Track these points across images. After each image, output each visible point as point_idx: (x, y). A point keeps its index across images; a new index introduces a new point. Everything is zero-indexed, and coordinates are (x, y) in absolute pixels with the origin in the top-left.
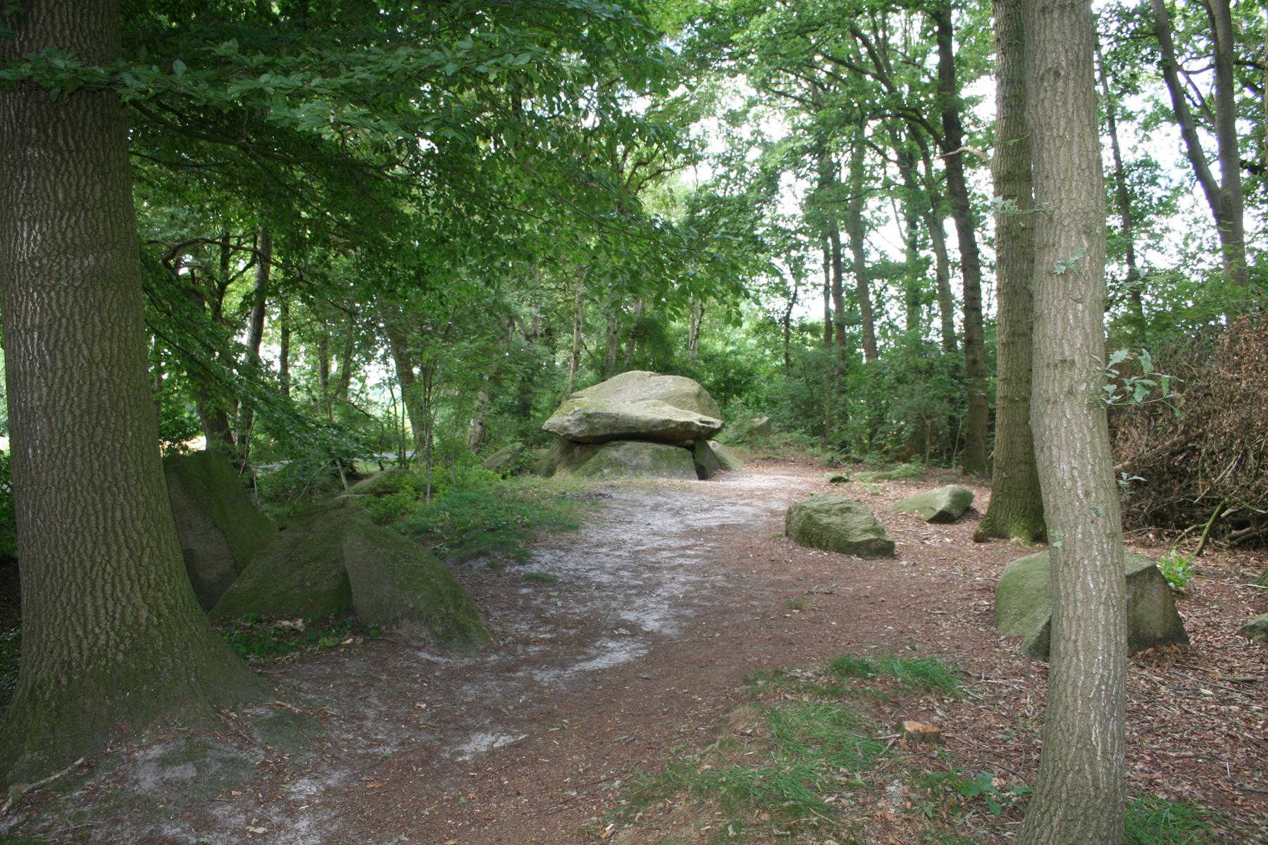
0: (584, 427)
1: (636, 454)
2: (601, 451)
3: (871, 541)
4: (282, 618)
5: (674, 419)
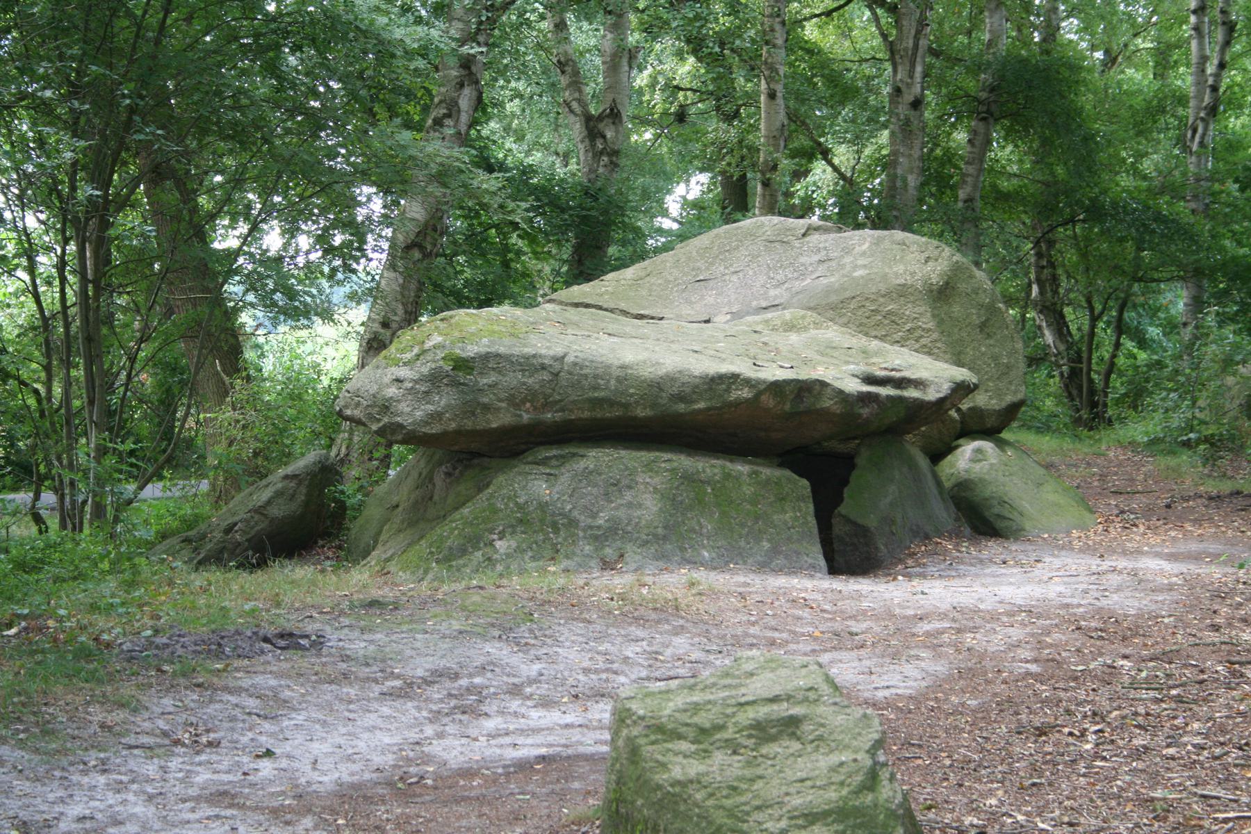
0: (444, 400)
1: (615, 487)
2: (501, 479)
5: (742, 368)
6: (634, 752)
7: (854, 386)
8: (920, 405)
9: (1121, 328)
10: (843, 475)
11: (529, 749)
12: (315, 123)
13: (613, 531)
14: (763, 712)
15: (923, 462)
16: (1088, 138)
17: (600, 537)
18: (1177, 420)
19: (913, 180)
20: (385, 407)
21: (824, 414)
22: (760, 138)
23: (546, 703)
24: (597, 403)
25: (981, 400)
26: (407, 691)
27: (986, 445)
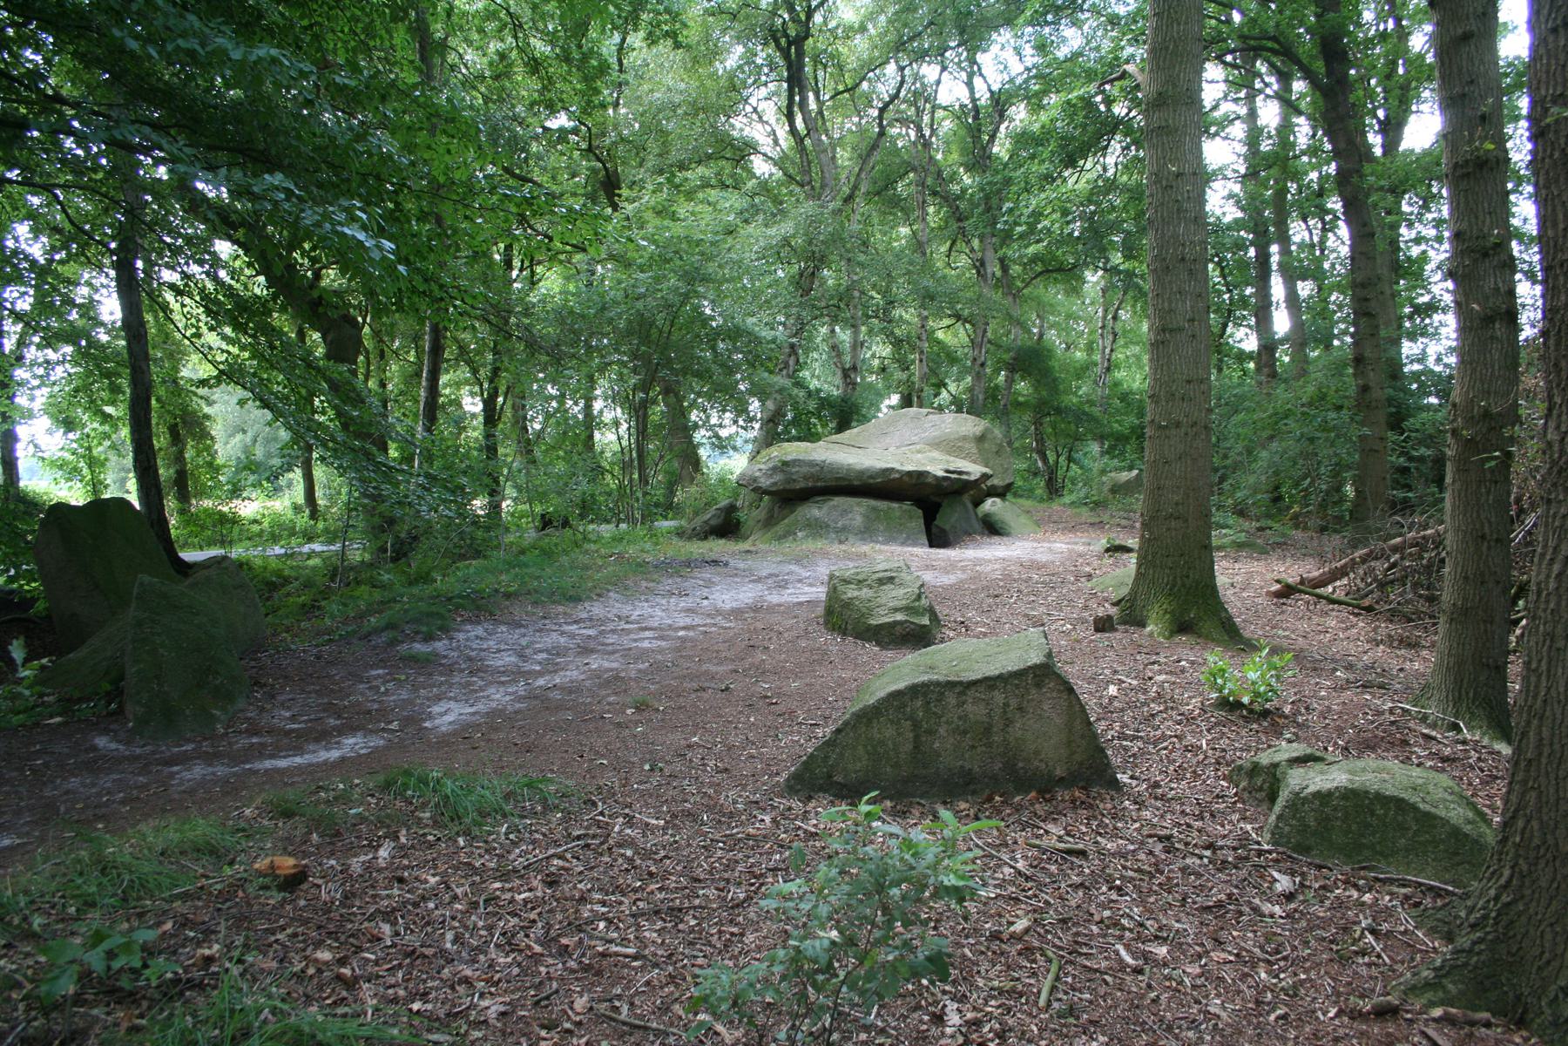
0: (778, 477)
1: (845, 512)
3: (896, 623)
4: (59, 724)
5: (897, 466)
6: (835, 588)
7: (941, 474)
8: (967, 482)
9: (1070, 459)
10: (936, 507)
11: (802, 599)
12: (731, 371)
13: (844, 529)
14: (881, 575)
15: (970, 506)
16: (1055, 380)
17: (839, 531)
18: (1082, 494)
19: (981, 397)
20: (755, 480)
21: (928, 484)
22: (916, 379)
23: (811, 585)
24: (838, 479)
25: (996, 481)
26: (759, 580)
27: (997, 500)
